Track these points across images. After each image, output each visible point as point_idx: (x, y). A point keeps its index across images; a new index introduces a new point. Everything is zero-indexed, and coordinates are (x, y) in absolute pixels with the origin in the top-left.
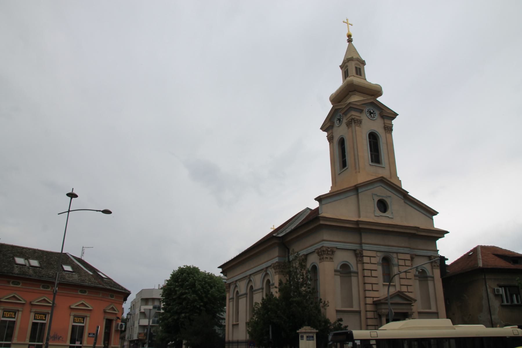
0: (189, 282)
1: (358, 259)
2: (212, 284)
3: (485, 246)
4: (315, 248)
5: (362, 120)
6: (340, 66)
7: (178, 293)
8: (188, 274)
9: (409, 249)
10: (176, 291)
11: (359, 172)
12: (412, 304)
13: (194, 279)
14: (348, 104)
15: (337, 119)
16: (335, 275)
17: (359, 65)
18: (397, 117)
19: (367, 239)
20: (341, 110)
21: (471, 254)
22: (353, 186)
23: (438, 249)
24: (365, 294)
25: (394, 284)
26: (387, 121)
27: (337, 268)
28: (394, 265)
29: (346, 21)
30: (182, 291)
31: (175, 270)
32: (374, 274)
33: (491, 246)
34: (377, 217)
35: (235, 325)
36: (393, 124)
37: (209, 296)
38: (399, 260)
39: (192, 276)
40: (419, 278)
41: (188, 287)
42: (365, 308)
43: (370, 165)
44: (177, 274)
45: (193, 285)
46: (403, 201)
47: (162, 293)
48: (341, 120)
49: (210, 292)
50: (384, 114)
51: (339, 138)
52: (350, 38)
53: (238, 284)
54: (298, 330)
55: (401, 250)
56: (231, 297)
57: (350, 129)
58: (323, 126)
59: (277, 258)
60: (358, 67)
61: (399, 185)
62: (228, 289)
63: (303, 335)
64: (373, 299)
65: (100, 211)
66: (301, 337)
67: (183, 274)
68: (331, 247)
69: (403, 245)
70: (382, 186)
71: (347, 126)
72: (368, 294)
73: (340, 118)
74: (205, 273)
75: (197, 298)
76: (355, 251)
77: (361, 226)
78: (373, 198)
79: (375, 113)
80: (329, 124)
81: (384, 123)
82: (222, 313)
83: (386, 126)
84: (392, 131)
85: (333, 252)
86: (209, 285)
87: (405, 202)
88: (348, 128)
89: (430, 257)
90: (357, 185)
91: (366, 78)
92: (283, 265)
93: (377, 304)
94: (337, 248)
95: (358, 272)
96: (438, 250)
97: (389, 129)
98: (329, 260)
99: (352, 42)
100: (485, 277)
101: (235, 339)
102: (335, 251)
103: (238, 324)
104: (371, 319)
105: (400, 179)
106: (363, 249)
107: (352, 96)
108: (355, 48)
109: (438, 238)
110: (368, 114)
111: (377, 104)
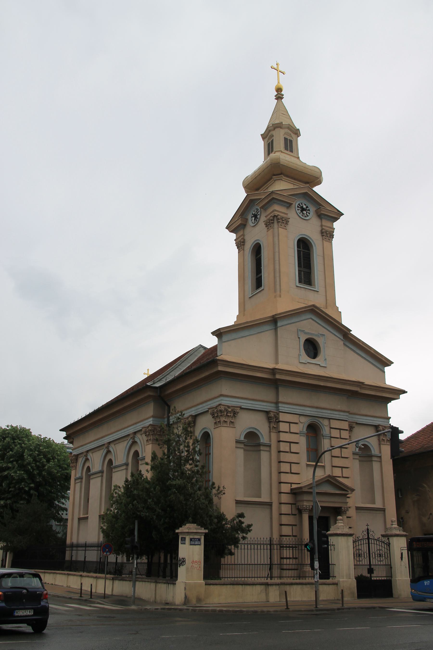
1: (272, 425)
5: (289, 218)
8: (13, 439)
9: (347, 414)
11: (280, 296)
12: (348, 496)
17: (291, 136)
18: (342, 217)
25: (323, 464)
26: (326, 223)
29: (275, 66)
32: (294, 448)
34: (303, 365)
35: (83, 520)
37: (44, 473)
42: (279, 498)
43: (297, 286)
45: (20, 456)
48: (258, 216)
52: (279, 92)
53: (90, 456)
55: (336, 415)
56: (78, 475)
59: (151, 419)
60: (289, 138)
62: (75, 464)
63: (184, 536)
64: (291, 486)
66: (181, 540)
69: (339, 407)
73: (257, 213)
75: (25, 476)
76: (267, 413)
77: (278, 376)
78: (298, 336)
79: (309, 210)
80: (239, 222)
81: (322, 226)
82: (63, 501)
83: (324, 231)
85: (235, 414)
86: (45, 456)
89: (376, 427)
94: (241, 408)
96: (390, 418)
106: (280, 411)
109: (390, 400)
110: (298, 210)
111: (313, 196)
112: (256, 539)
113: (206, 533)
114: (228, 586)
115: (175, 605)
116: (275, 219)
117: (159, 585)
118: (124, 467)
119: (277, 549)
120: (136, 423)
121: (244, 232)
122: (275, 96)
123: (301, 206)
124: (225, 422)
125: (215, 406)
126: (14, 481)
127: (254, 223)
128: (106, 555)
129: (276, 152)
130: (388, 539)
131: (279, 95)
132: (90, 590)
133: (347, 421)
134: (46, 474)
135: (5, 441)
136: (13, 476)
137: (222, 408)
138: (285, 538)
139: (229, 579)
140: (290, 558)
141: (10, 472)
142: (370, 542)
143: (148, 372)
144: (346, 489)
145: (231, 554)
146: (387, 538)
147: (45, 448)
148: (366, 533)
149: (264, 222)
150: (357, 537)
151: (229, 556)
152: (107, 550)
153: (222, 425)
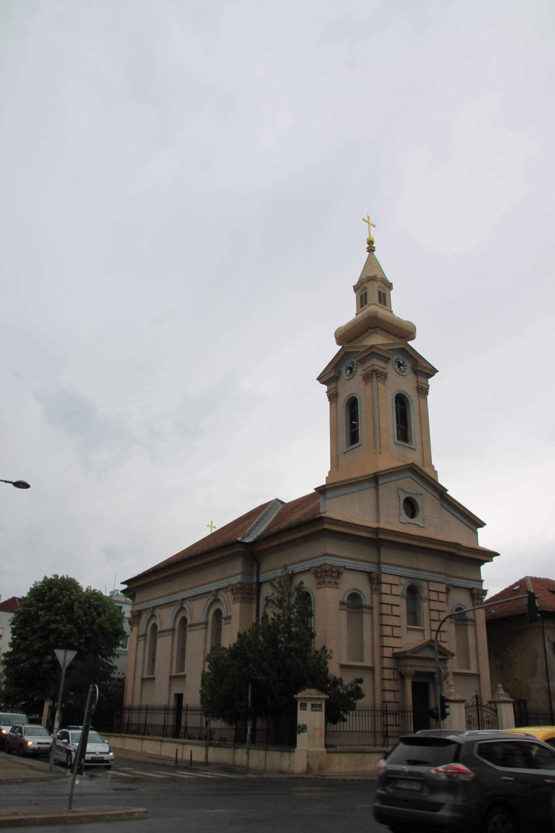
0: (63, 603)
2: (100, 609)
3: (535, 577)
4: (310, 565)
5: (388, 373)
6: (354, 287)
7: (42, 620)
8: (61, 589)
9: (444, 576)
10: (38, 617)
11: (380, 453)
13: (70, 599)
14: (369, 348)
15: (347, 367)
16: (341, 609)
17: (384, 290)
18: (437, 374)
19: (388, 556)
20: (358, 354)
21: (517, 588)
22: (371, 474)
23: (482, 579)
24: (381, 641)
25: (422, 628)
26: (421, 379)
27: (343, 599)
28: (423, 600)
29: (367, 219)
30: (50, 617)
31: (38, 582)
32: (396, 611)
33: (544, 578)
34: (403, 524)
35: (148, 680)
36: (429, 384)
37: (95, 628)
38: (430, 592)
39: (68, 593)
40: (348, 607)
41: (59, 612)
42: (382, 663)
43: (396, 443)
44: (41, 588)
45: (69, 609)
46: (438, 503)
47: (12, 619)
48: (354, 370)
49: (98, 621)
50: (419, 369)
51: (348, 396)
52: (371, 245)
53: (157, 612)
54: (297, 694)
55: (435, 577)
57: (369, 385)
58: (319, 378)
59: (239, 576)
60: (382, 291)
61: (434, 478)
62: (138, 620)
63: (305, 702)
64: (393, 650)
65: (10, 482)
67: (50, 589)
68: (338, 565)
69: (436, 569)
70: (412, 478)
71: (364, 381)
72: (387, 642)
73: (353, 366)
74: (90, 590)
75: (75, 630)
76: (369, 573)
77: (381, 536)
78: (398, 495)
79: (405, 366)
80: (333, 374)
81: (418, 382)
82: (112, 659)
83: (420, 387)
84: (428, 394)
85: (339, 574)
86: (96, 610)
87: (441, 505)
88: (366, 383)
89: (471, 590)
90: (378, 472)
91: (393, 309)
92: (248, 587)
93: (398, 657)
94: (345, 568)
95: (373, 606)
97: (423, 391)
98: (333, 586)
99: (374, 253)
100: (543, 624)
101: (146, 702)
102: (342, 573)
103: (154, 679)
104: (389, 681)
105: (436, 469)
106: (382, 572)
107: (372, 335)
108: (378, 262)
109: (482, 562)
110: (395, 365)
112: (367, 705)
113: (326, 699)
114: (348, 755)
115: (293, 773)
116: (374, 373)
117: (270, 753)
118: (203, 626)
119: (371, 716)
120: (219, 580)
121: (336, 384)
122: (367, 248)
123: (398, 361)
124: (330, 582)
125: (318, 565)
126: (63, 636)
127: (349, 376)
128: (209, 720)
129: (371, 305)
130: (496, 705)
131: (371, 248)
132: (175, 757)
133: (443, 583)
134: (97, 628)
135: (53, 592)
136: (61, 630)
137: (327, 568)
138: (388, 704)
139: (348, 747)
140: (393, 725)
141: (59, 626)
142: (386, 708)
143: (212, 524)
144: (445, 653)
145: (344, 720)
146: (494, 705)
147: (95, 601)
148: (475, 699)
149: (362, 375)
150: (468, 704)
151: (342, 723)
152: (210, 715)
153: (326, 585)
